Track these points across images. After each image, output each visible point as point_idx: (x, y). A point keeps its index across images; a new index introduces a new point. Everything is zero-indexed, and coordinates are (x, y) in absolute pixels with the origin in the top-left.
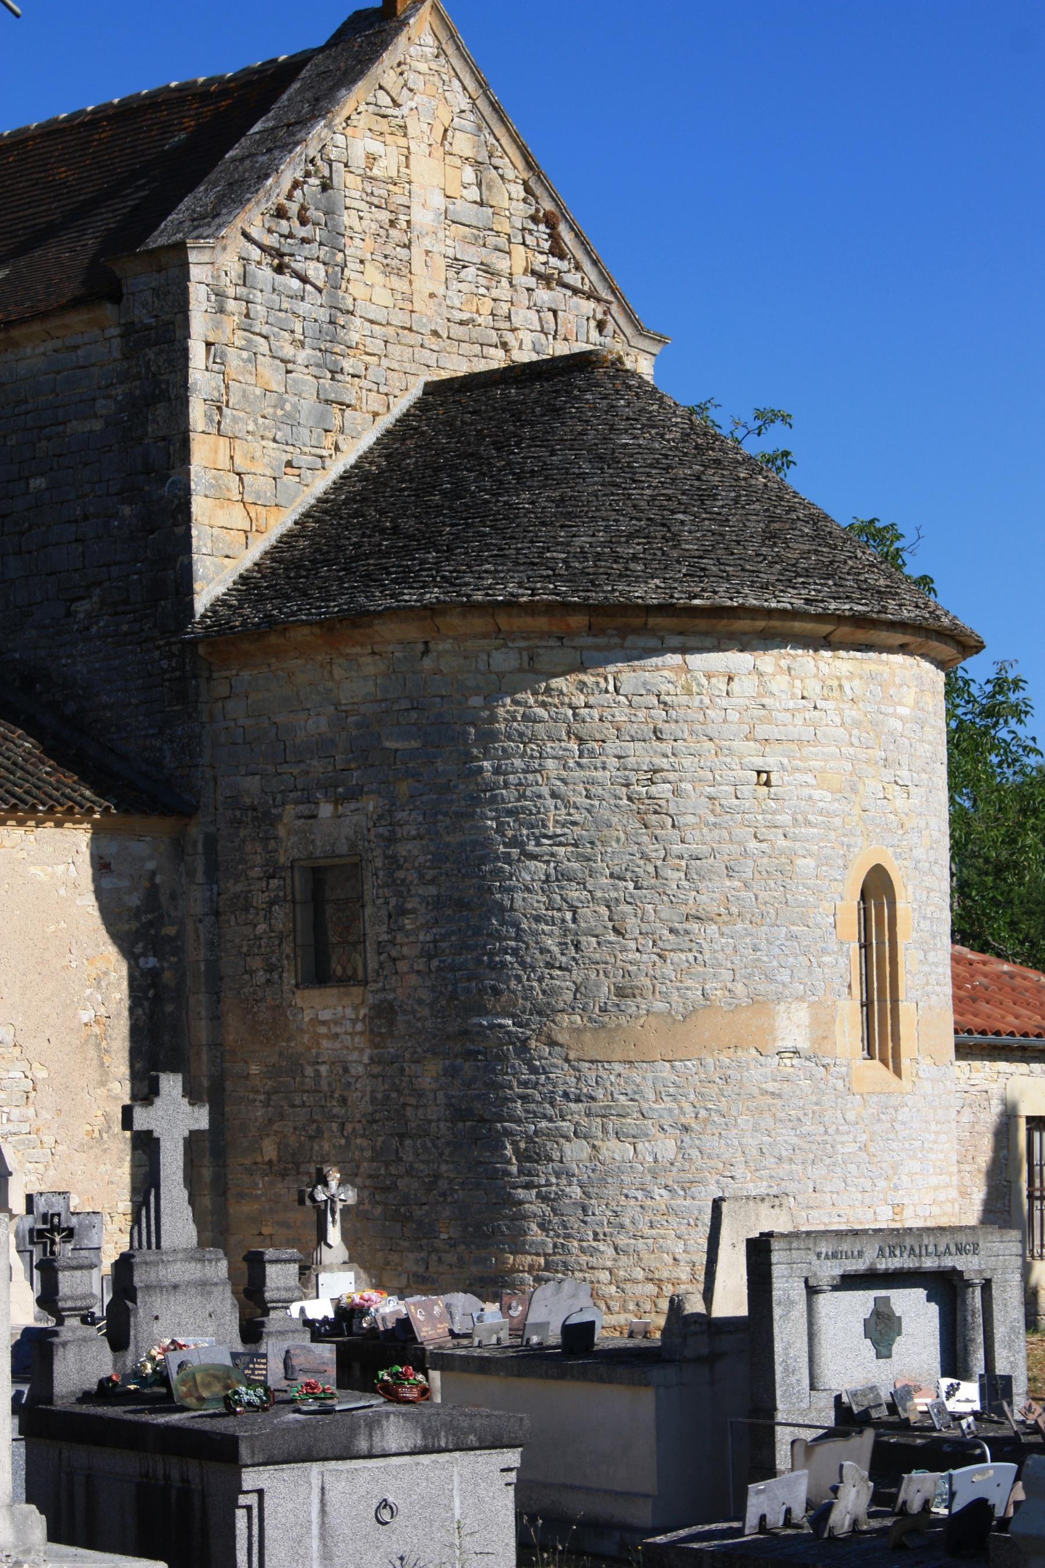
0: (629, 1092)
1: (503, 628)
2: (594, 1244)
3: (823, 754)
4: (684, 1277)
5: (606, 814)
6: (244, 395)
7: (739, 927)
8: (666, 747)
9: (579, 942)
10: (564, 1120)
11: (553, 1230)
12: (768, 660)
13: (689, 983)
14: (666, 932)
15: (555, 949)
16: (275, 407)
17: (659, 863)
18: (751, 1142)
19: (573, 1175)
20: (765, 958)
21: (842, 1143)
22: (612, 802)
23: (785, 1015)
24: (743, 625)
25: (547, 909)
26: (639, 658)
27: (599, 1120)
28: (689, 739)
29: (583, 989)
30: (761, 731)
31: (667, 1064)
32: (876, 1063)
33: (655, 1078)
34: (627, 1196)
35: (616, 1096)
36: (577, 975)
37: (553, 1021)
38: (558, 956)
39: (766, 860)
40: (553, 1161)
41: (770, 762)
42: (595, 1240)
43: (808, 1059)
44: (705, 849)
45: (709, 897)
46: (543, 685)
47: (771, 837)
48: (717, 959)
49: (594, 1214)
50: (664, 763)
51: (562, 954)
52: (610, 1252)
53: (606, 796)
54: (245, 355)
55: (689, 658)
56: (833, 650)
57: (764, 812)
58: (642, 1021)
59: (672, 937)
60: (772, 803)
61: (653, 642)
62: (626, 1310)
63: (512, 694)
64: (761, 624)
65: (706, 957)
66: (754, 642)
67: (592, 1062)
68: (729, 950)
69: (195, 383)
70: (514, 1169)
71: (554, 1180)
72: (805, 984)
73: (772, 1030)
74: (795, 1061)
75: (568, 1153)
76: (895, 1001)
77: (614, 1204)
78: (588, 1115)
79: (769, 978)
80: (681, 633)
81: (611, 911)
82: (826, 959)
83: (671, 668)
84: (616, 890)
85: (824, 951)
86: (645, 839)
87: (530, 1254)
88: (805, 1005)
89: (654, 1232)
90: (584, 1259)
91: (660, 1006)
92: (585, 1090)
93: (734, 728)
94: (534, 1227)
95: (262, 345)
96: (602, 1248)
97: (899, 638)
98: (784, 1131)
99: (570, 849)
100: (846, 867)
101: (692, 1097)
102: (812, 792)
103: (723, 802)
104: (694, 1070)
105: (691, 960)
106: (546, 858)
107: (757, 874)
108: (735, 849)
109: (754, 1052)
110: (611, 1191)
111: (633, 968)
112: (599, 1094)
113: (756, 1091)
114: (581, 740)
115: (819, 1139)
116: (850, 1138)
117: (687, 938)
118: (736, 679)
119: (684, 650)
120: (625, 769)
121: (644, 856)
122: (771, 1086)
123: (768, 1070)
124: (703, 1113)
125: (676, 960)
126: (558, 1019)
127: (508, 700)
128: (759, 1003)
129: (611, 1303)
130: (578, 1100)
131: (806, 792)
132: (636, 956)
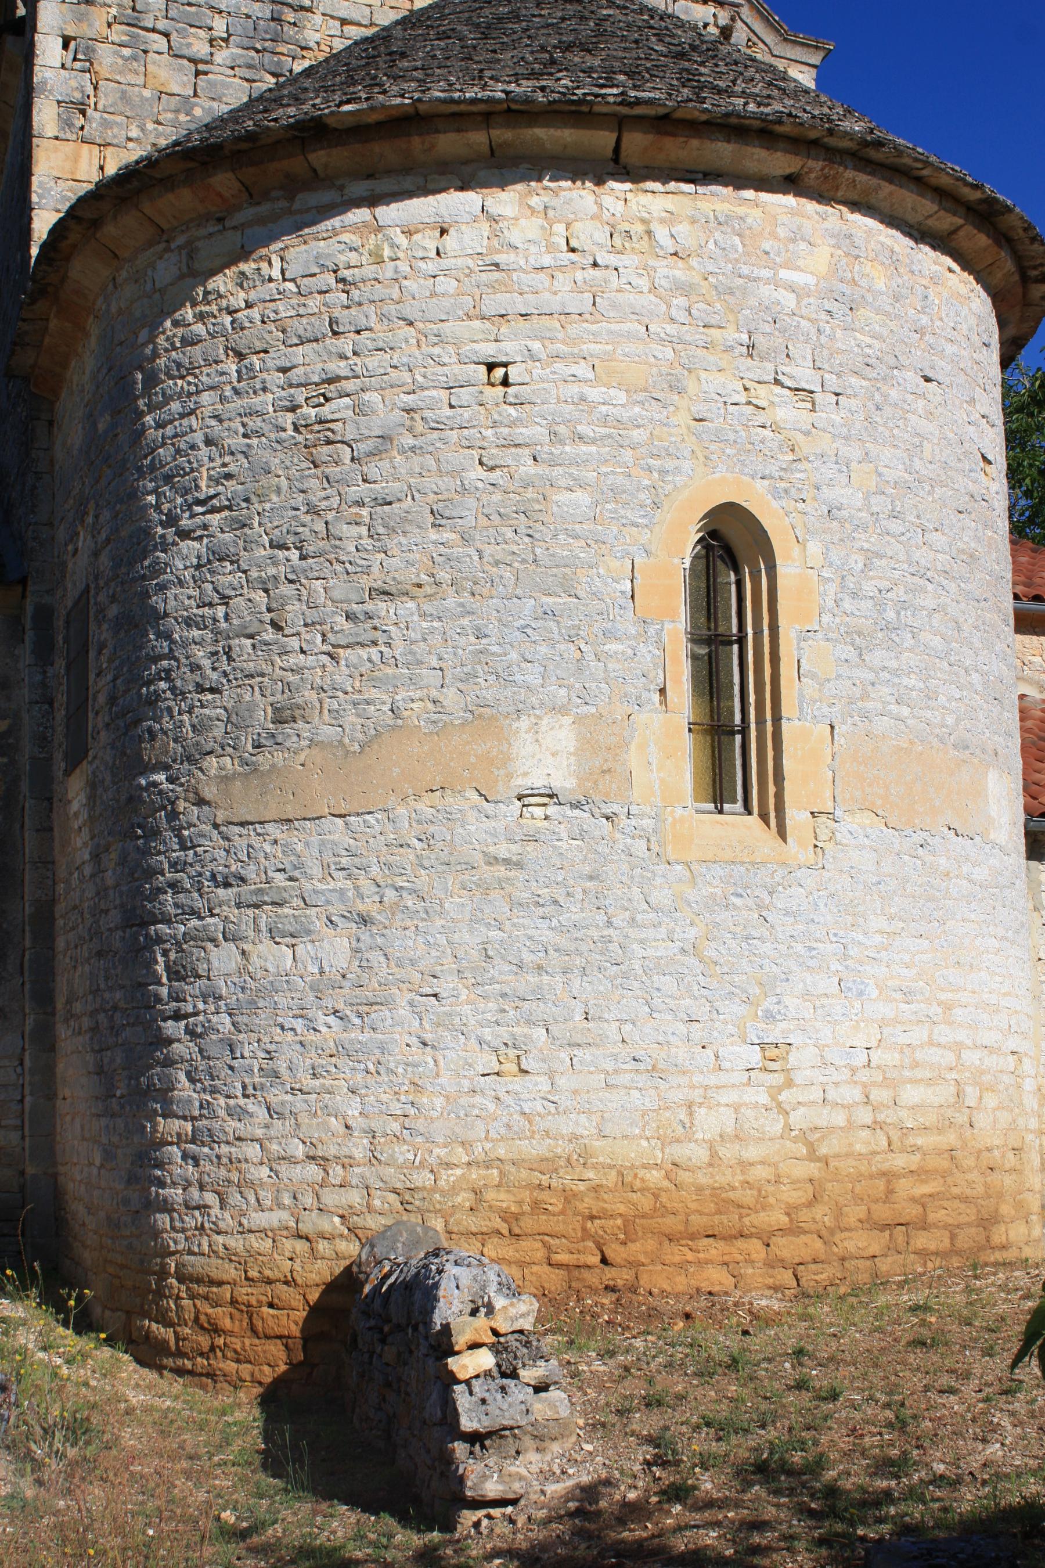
0: (288, 867)
1: (165, 227)
2: (242, 1101)
3: (610, 332)
4: (359, 1154)
5: (266, 455)
6: (124, 96)
7: (451, 602)
8: (346, 345)
9: (230, 647)
10: (212, 915)
11: (200, 1080)
12: (506, 201)
13: (374, 694)
14: (341, 620)
15: (206, 663)
16: (177, 111)
17: (330, 516)
18: (469, 940)
19: (220, 998)
20: (495, 649)
21: (642, 942)
22: (273, 436)
23: (529, 737)
24: (448, 143)
25: (198, 607)
26: (314, 223)
27: (250, 912)
28: (378, 327)
29: (234, 718)
30: (491, 304)
31: (339, 821)
32: (754, 819)
33: (323, 843)
34: (283, 1028)
35: (270, 874)
36: (227, 698)
37: (201, 769)
38: (209, 672)
39: (497, 497)
40: (199, 977)
41: (508, 349)
42: (245, 1096)
43: (577, 805)
44: (395, 488)
45: (404, 559)
46: (200, 290)
47: (509, 461)
48: (412, 653)
49: (243, 1057)
50: (340, 368)
51: (214, 669)
52: (262, 1113)
53: (266, 428)
54: (126, 52)
55: (381, 211)
56: (634, 181)
57: (495, 425)
58: (302, 757)
59: (348, 626)
60: (511, 410)
61: (327, 196)
62: (280, 1206)
63: (170, 314)
64: (478, 138)
65: (397, 654)
66: (482, 174)
67: (242, 824)
68: (436, 640)
69: (45, 83)
70: (164, 991)
71: (201, 1006)
72: (570, 688)
73: (507, 759)
74: (551, 810)
75: (215, 963)
76: (777, 719)
77: (266, 1039)
78: (238, 906)
79: (504, 678)
80: (370, 176)
81: (269, 596)
82: (612, 647)
83: (354, 228)
84: (275, 564)
85: (609, 635)
86: (313, 483)
87: (178, 1117)
88: (567, 720)
89: (317, 1083)
90: (232, 1125)
91: (328, 732)
92: (233, 869)
93: (446, 303)
94: (182, 1076)
95: (159, 42)
96: (251, 1108)
97: (781, 163)
98: (526, 921)
99: (226, 513)
100: (656, 505)
101: (375, 870)
102: (587, 390)
103: (427, 414)
104: (378, 828)
105: (376, 658)
106: (198, 533)
107: (483, 521)
108: (447, 483)
109: (475, 796)
110: (262, 1019)
111: (291, 677)
112: (250, 872)
113: (478, 858)
114: (240, 356)
115: (595, 934)
116: (662, 932)
117: (368, 625)
118: (452, 231)
119: (373, 201)
120: (291, 386)
121: (313, 511)
122: (504, 850)
123: (499, 825)
124: (390, 895)
125: (354, 659)
126: (205, 764)
127: (168, 324)
128: (483, 719)
129: (262, 1194)
130: (227, 885)
131: (573, 390)
132: (303, 661)
